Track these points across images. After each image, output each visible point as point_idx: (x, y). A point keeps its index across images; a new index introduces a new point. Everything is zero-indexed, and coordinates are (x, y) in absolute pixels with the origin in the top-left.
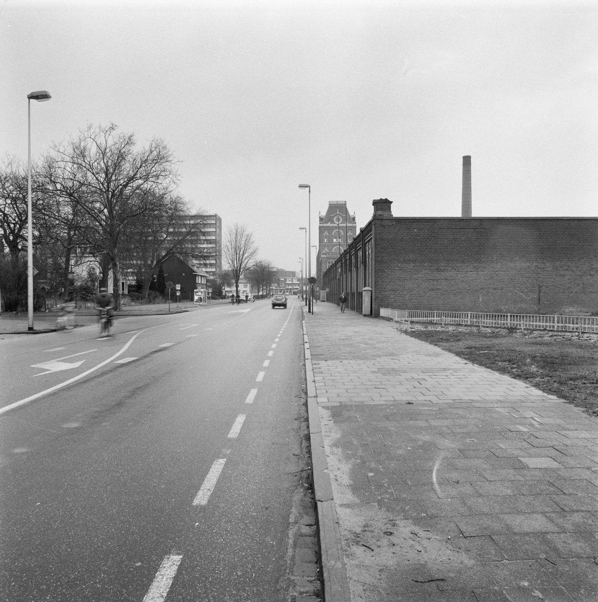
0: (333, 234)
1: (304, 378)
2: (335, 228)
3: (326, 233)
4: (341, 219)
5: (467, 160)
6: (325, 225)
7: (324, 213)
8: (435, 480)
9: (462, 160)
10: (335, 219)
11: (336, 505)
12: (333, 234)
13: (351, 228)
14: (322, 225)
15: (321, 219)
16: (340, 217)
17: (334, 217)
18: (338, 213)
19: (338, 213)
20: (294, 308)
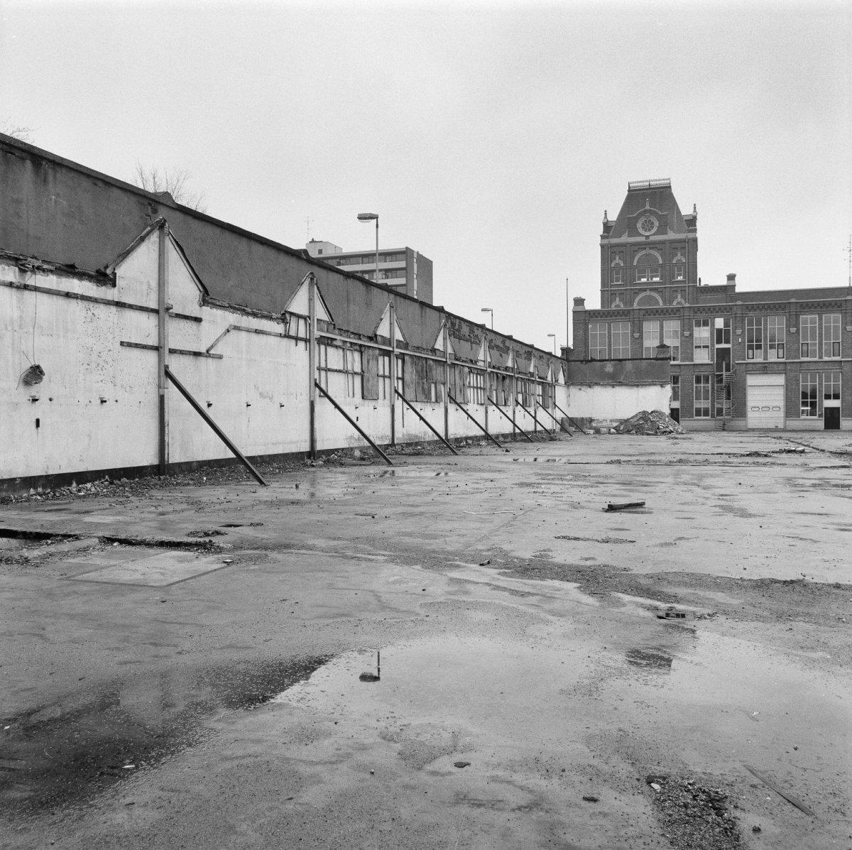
1: (752, 596)
2: (641, 246)
3: (617, 260)
4: (657, 224)
6: (615, 241)
7: (613, 216)
8: (415, 281)
10: (639, 225)
14: (606, 241)
15: (607, 227)
16: (654, 219)
17: (637, 219)
18: (647, 207)
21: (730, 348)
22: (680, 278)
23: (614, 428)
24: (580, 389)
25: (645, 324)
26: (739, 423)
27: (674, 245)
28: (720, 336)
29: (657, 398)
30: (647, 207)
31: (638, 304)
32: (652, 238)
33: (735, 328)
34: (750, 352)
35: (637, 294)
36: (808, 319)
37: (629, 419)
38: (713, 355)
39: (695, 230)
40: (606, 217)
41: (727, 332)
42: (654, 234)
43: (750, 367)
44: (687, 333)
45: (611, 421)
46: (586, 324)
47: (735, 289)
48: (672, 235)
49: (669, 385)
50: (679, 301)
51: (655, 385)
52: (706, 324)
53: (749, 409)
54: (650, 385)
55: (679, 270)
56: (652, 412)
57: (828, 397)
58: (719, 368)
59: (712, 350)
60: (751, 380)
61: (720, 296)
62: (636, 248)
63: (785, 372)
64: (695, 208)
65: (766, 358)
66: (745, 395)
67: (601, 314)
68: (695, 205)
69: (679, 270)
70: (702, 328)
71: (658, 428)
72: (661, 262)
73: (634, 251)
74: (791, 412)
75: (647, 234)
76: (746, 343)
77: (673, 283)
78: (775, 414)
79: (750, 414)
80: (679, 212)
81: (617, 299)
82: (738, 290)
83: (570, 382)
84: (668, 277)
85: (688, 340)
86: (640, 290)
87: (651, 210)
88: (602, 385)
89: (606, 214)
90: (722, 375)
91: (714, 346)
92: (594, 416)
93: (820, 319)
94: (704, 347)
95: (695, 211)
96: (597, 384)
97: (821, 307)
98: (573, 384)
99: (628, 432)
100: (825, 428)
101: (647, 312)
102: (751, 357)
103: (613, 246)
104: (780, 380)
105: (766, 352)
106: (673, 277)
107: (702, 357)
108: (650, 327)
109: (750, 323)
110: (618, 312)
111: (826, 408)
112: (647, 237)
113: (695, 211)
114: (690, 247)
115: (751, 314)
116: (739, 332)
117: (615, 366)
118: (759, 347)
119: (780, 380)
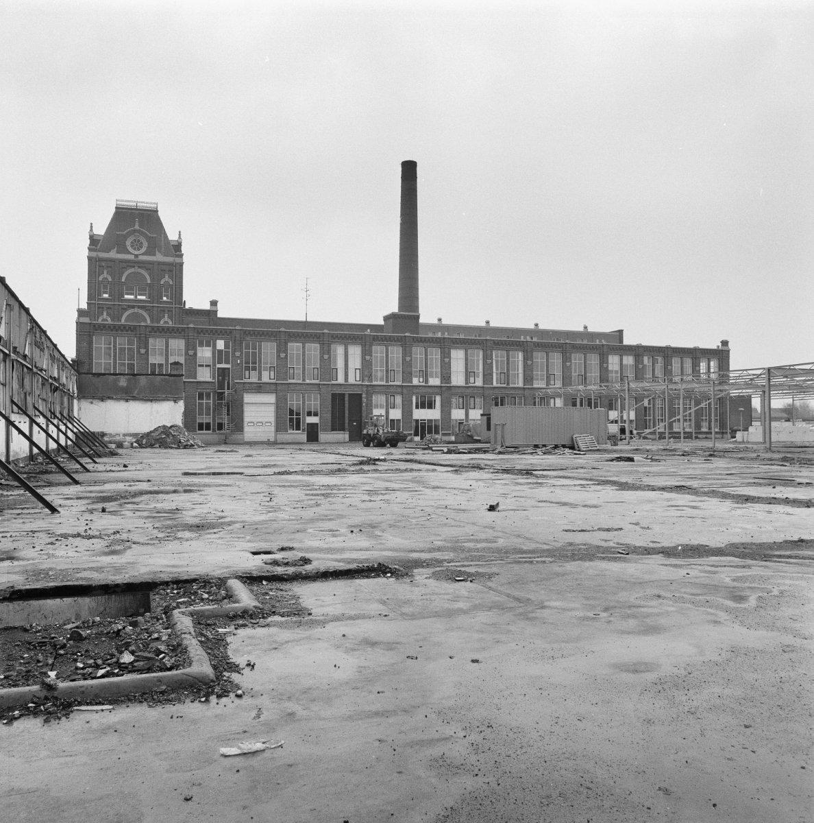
0: (123, 280)
3: (105, 275)
4: (145, 244)
5: (409, 169)
7: (101, 230)
9: (400, 169)
10: (128, 243)
11: (751, 819)
12: (123, 280)
13: (110, 264)
14: (94, 254)
15: (94, 240)
17: (125, 237)
19: (137, 227)
20: (33, 564)
21: (229, 369)
22: (106, 296)
23: (135, 442)
24: (92, 403)
25: (151, 341)
26: (237, 437)
27: (164, 267)
28: (219, 356)
29: (169, 413)
30: (137, 227)
31: (126, 321)
32: (141, 258)
33: (234, 351)
34: (247, 372)
35: (125, 310)
36: (294, 347)
37: (151, 432)
38: (214, 374)
39: (181, 256)
40: (91, 230)
41: (227, 353)
42: (142, 254)
43: (247, 386)
44: (191, 353)
45: (124, 435)
46: (90, 337)
47: (217, 314)
48: (159, 257)
49: (182, 401)
50: (105, 317)
51: (168, 400)
52: (208, 345)
53: (245, 424)
54: (164, 400)
55: (105, 287)
56: (171, 427)
57: (309, 414)
58: (221, 386)
59: (214, 369)
60: (248, 398)
61: (202, 319)
62: (125, 265)
63: (276, 391)
64: (180, 235)
65: (260, 378)
66: (242, 411)
67: (117, 328)
68: (91, 224)
69: (105, 287)
70: (205, 348)
71: (180, 442)
72: (149, 282)
73: (123, 268)
74: (279, 428)
75: (136, 253)
76: (244, 365)
77: (99, 299)
78: (267, 429)
79: (246, 429)
80: (166, 237)
81: (166, 316)
82: (220, 315)
83: (79, 399)
84: (155, 296)
85: (192, 359)
86: (129, 306)
87: (140, 230)
88: (115, 399)
89: (91, 227)
90: (224, 392)
91: (215, 366)
92: (106, 430)
93: (304, 347)
94: (206, 366)
95: (180, 237)
96: (109, 398)
97: (261, 336)
98: (84, 397)
99: (152, 446)
100: (307, 441)
101: (153, 329)
102: (247, 377)
103: (101, 260)
104: (271, 398)
105: (260, 374)
106: (100, 294)
107: (204, 375)
108: (156, 343)
109: (247, 347)
110: (104, 326)
111: (308, 424)
112: (136, 256)
113: (180, 237)
114: (176, 270)
115: (248, 338)
116: (238, 354)
117: (129, 380)
118: (254, 369)
119: (271, 398)
